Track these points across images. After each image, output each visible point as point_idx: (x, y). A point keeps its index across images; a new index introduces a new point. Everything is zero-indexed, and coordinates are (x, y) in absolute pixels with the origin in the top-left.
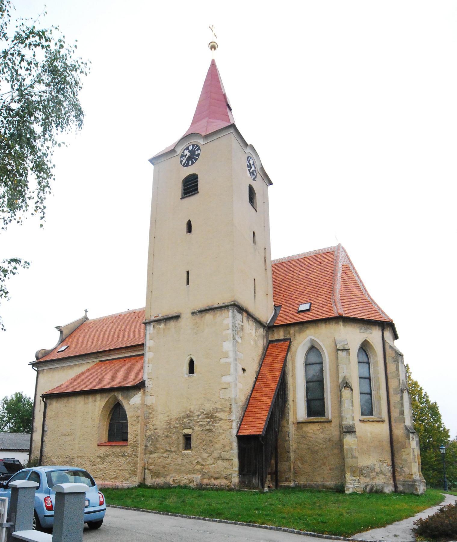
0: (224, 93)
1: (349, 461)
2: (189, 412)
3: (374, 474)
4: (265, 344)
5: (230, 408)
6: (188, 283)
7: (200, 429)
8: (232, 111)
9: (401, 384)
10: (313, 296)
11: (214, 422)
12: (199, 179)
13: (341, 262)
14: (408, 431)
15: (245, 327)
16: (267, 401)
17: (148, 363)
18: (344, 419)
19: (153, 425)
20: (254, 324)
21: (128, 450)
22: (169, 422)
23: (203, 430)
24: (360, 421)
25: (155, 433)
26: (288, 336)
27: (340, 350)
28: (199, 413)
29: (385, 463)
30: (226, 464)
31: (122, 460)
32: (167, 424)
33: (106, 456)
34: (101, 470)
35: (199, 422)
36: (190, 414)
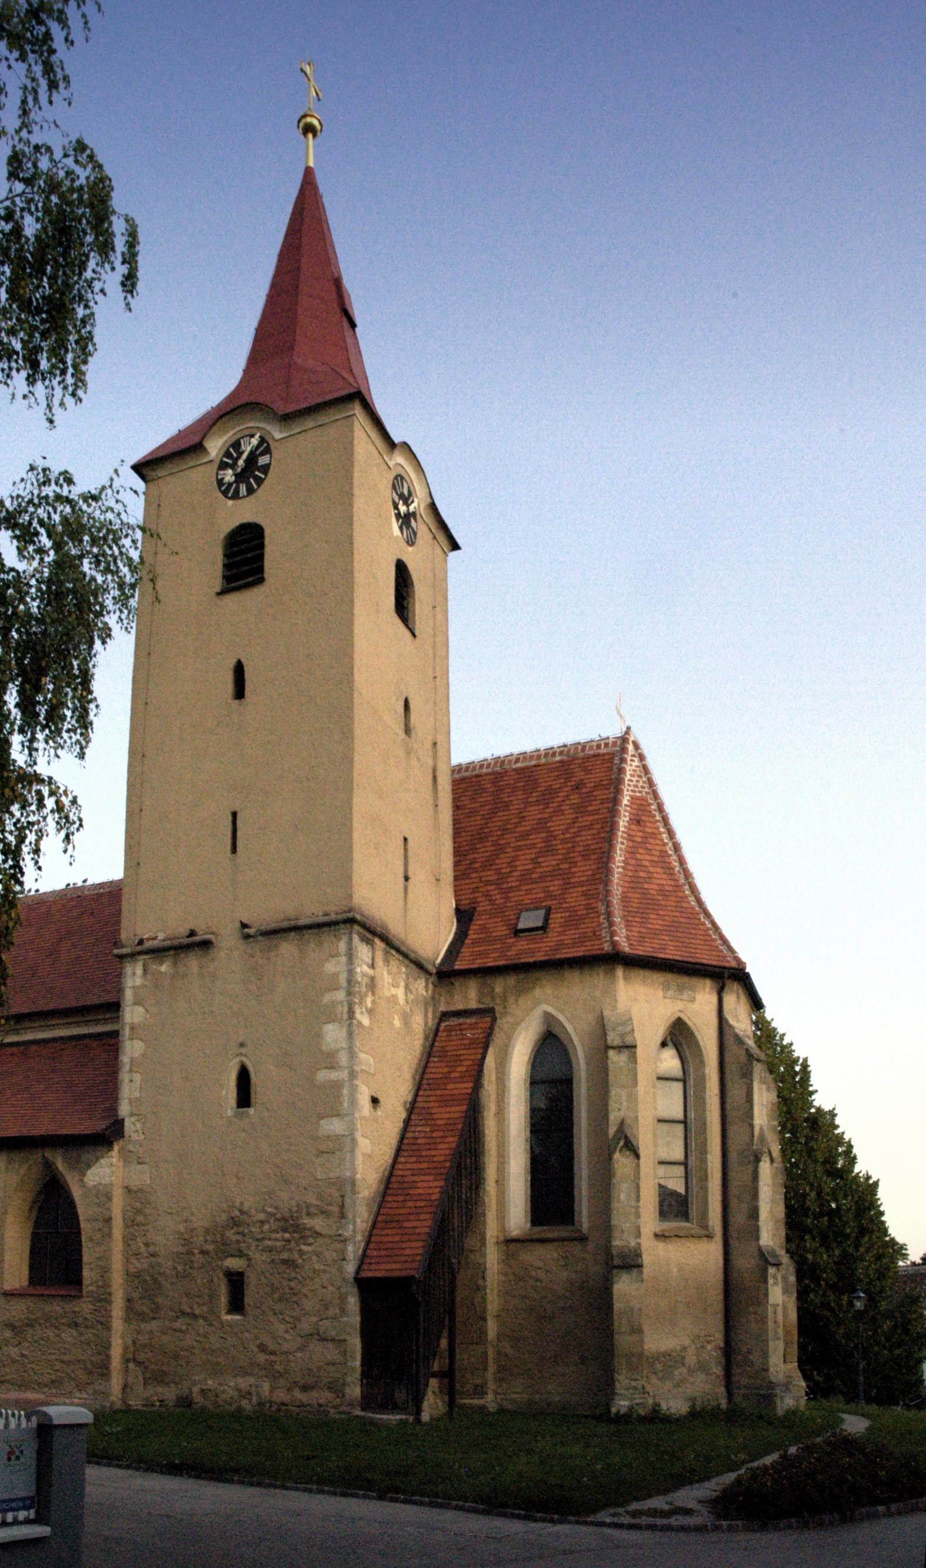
0: (336, 275)
1: (623, 1341)
2: (238, 1214)
3: (684, 1370)
4: (430, 1024)
5: (342, 1206)
6: (234, 849)
7: (266, 1257)
8: (357, 330)
9: (756, 1138)
10: (555, 886)
11: (302, 1241)
12: (267, 541)
13: (630, 788)
14: (766, 1260)
15: (379, 982)
16: (431, 1187)
17: (131, 1071)
18: (616, 1234)
19: (147, 1245)
20: (404, 969)
21: (84, 1307)
22: (187, 1237)
23: (273, 1260)
24: (656, 1235)
25: (151, 1266)
26: (488, 1003)
27: (613, 1048)
28: (262, 1216)
29: (708, 1342)
30: (332, 1353)
31: (69, 1335)
32: (183, 1242)
33: (28, 1325)
34: (14, 1361)
35: (263, 1239)
36: (241, 1217)
